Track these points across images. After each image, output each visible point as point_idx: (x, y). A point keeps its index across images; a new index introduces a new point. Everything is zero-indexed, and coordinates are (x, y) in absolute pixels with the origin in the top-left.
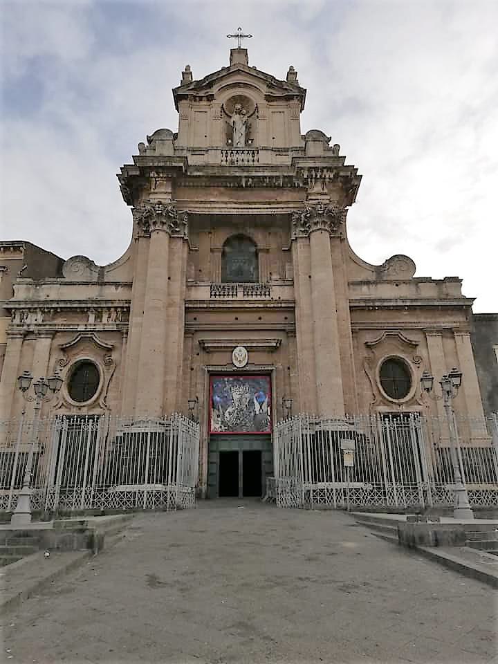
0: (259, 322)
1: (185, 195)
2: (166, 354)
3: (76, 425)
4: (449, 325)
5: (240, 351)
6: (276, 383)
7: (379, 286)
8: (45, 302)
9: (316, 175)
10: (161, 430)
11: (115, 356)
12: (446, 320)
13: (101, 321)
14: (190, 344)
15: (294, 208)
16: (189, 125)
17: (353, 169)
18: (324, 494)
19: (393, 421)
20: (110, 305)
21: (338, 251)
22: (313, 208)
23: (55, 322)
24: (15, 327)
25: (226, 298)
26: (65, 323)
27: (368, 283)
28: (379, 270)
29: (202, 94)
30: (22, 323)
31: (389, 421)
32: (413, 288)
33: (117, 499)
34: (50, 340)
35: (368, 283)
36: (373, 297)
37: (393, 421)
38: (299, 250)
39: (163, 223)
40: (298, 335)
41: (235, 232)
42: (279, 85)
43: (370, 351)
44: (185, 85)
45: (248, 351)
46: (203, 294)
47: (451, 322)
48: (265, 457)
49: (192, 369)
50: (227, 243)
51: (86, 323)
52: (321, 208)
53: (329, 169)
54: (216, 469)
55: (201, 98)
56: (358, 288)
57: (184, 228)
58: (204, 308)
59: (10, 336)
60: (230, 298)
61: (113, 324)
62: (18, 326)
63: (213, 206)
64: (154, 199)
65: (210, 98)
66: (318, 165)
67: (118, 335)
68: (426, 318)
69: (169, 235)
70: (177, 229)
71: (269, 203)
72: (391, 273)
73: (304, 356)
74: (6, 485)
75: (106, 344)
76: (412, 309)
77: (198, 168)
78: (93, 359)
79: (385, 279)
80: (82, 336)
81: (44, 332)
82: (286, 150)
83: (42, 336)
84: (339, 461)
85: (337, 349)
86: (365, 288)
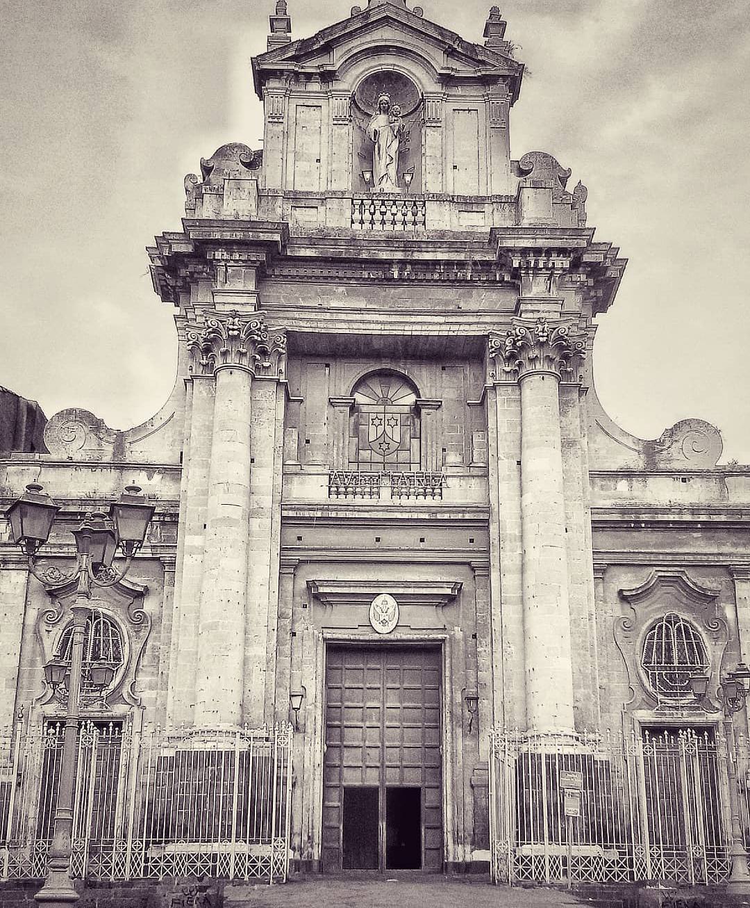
0: (422, 546)
1: (279, 294)
7: (650, 480)
9: (536, 262)
10: (240, 746)
11: (149, 606)
15: (494, 324)
16: (286, 134)
17: (611, 250)
19: (651, 741)
21: (573, 412)
25: (358, 500)
27: (628, 474)
28: (651, 449)
32: (714, 484)
35: (628, 474)
37: (651, 741)
38: (501, 411)
39: (242, 354)
40: (494, 575)
41: (374, 367)
42: (469, 53)
43: (627, 606)
44: (278, 46)
48: (428, 799)
53: (562, 251)
55: (309, 77)
57: (280, 360)
60: (367, 500)
64: (226, 303)
65: (327, 77)
66: (540, 243)
67: (154, 566)
68: (735, 545)
69: (249, 372)
70: (266, 364)
72: (675, 455)
73: (507, 616)
74: (155, 836)
75: (134, 584)
76: (709, 527)
77: (312, 242)
79: (662, 466)
83: (11, 566)
84: (557, 811)
85: (564, 603)
86: (623, 485)
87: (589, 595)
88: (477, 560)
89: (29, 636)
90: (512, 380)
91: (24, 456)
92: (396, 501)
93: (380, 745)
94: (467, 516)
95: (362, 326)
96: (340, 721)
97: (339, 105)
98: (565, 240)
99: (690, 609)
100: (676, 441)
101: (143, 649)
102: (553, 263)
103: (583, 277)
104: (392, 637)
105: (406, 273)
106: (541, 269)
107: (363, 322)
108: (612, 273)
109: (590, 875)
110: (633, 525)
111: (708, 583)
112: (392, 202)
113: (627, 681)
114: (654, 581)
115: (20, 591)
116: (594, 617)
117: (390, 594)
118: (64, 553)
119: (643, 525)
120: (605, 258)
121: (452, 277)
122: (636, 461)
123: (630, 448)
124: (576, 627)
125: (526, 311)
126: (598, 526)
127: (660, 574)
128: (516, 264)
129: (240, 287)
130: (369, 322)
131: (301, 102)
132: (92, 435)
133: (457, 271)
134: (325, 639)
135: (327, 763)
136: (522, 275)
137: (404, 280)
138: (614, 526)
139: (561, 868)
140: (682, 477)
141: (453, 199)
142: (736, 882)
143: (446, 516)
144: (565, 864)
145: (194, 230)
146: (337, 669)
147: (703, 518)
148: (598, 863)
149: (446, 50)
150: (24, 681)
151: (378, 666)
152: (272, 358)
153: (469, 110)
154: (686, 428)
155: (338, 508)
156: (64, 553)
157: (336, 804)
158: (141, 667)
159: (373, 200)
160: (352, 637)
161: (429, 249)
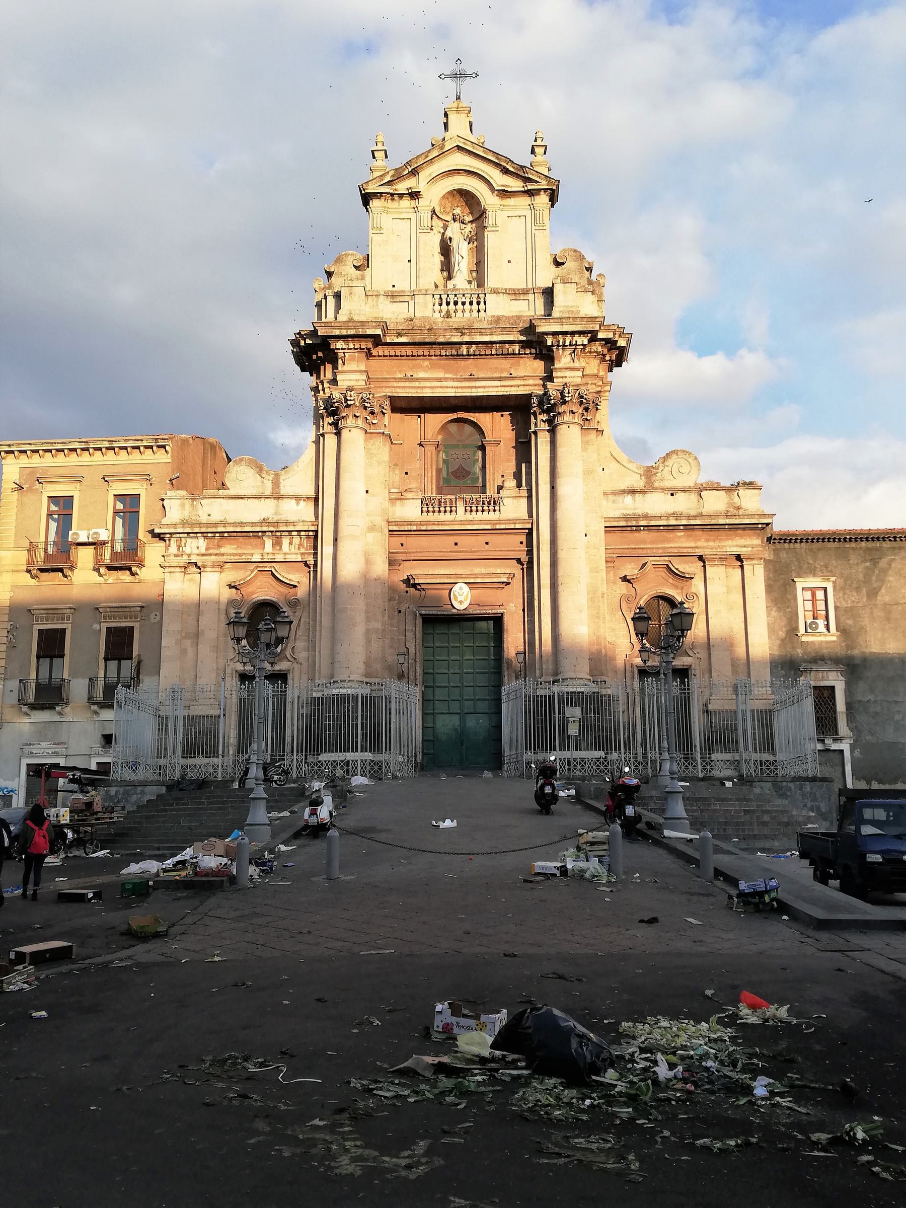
3: (281, 691)
4: (736, 551)
7: (648, 495)
8: (208, 525)
9: (564, 342)
10: (367, 691)
12: (735, 543)
13: (281, 549)
20: (291, 528)
23: (223, 550)
26: (235, 551)
27: (632, 492)
30: (180, 553)
32: (694, 497)
33: (594, 767)
35: (632, 492)
36: (639, 512)
46: (411, 511)
49: (400, 612)
51: (262, 552)
53: (580, 333)
56: (619, 498)
62: (176, 556)
68: (707, 540)
71: (500, 379)
74: (191, 754)
79: (656, 485)
80: (259, 569)
82: (525, 291)
86: (628, 499)
87: (602, 580)
91: (213, 492)
93: (460, 685)
94: (518, 526)
95: (441, 390)
100: (667, 466)
102: (576, 341)
103: (600, 349)
106: (567, 346)
108: (622, 343)
111: (688, 568)
117: (465, 583)
120: (615, 334)
121: (505, 352)
122: (638, 482)
125: (557, 377)
126: (609, 529)
128: (549, 343)
130: (447, 387)
132: (257, 475)
134: (421, 615)
135: (425, 698)
139: (567, 767)
141: (506, 291)
142: (662, 776)
143: (503, 527)
144: (569, 764)
145: (321, 329)
146: (430, 634)
147: (684, 522)
148: (327, 765)
149: (502, 170)
153: (520, 216)
154: (674, 456)
155: (427, 523)
158: (297, 636)
161: (488, 333)
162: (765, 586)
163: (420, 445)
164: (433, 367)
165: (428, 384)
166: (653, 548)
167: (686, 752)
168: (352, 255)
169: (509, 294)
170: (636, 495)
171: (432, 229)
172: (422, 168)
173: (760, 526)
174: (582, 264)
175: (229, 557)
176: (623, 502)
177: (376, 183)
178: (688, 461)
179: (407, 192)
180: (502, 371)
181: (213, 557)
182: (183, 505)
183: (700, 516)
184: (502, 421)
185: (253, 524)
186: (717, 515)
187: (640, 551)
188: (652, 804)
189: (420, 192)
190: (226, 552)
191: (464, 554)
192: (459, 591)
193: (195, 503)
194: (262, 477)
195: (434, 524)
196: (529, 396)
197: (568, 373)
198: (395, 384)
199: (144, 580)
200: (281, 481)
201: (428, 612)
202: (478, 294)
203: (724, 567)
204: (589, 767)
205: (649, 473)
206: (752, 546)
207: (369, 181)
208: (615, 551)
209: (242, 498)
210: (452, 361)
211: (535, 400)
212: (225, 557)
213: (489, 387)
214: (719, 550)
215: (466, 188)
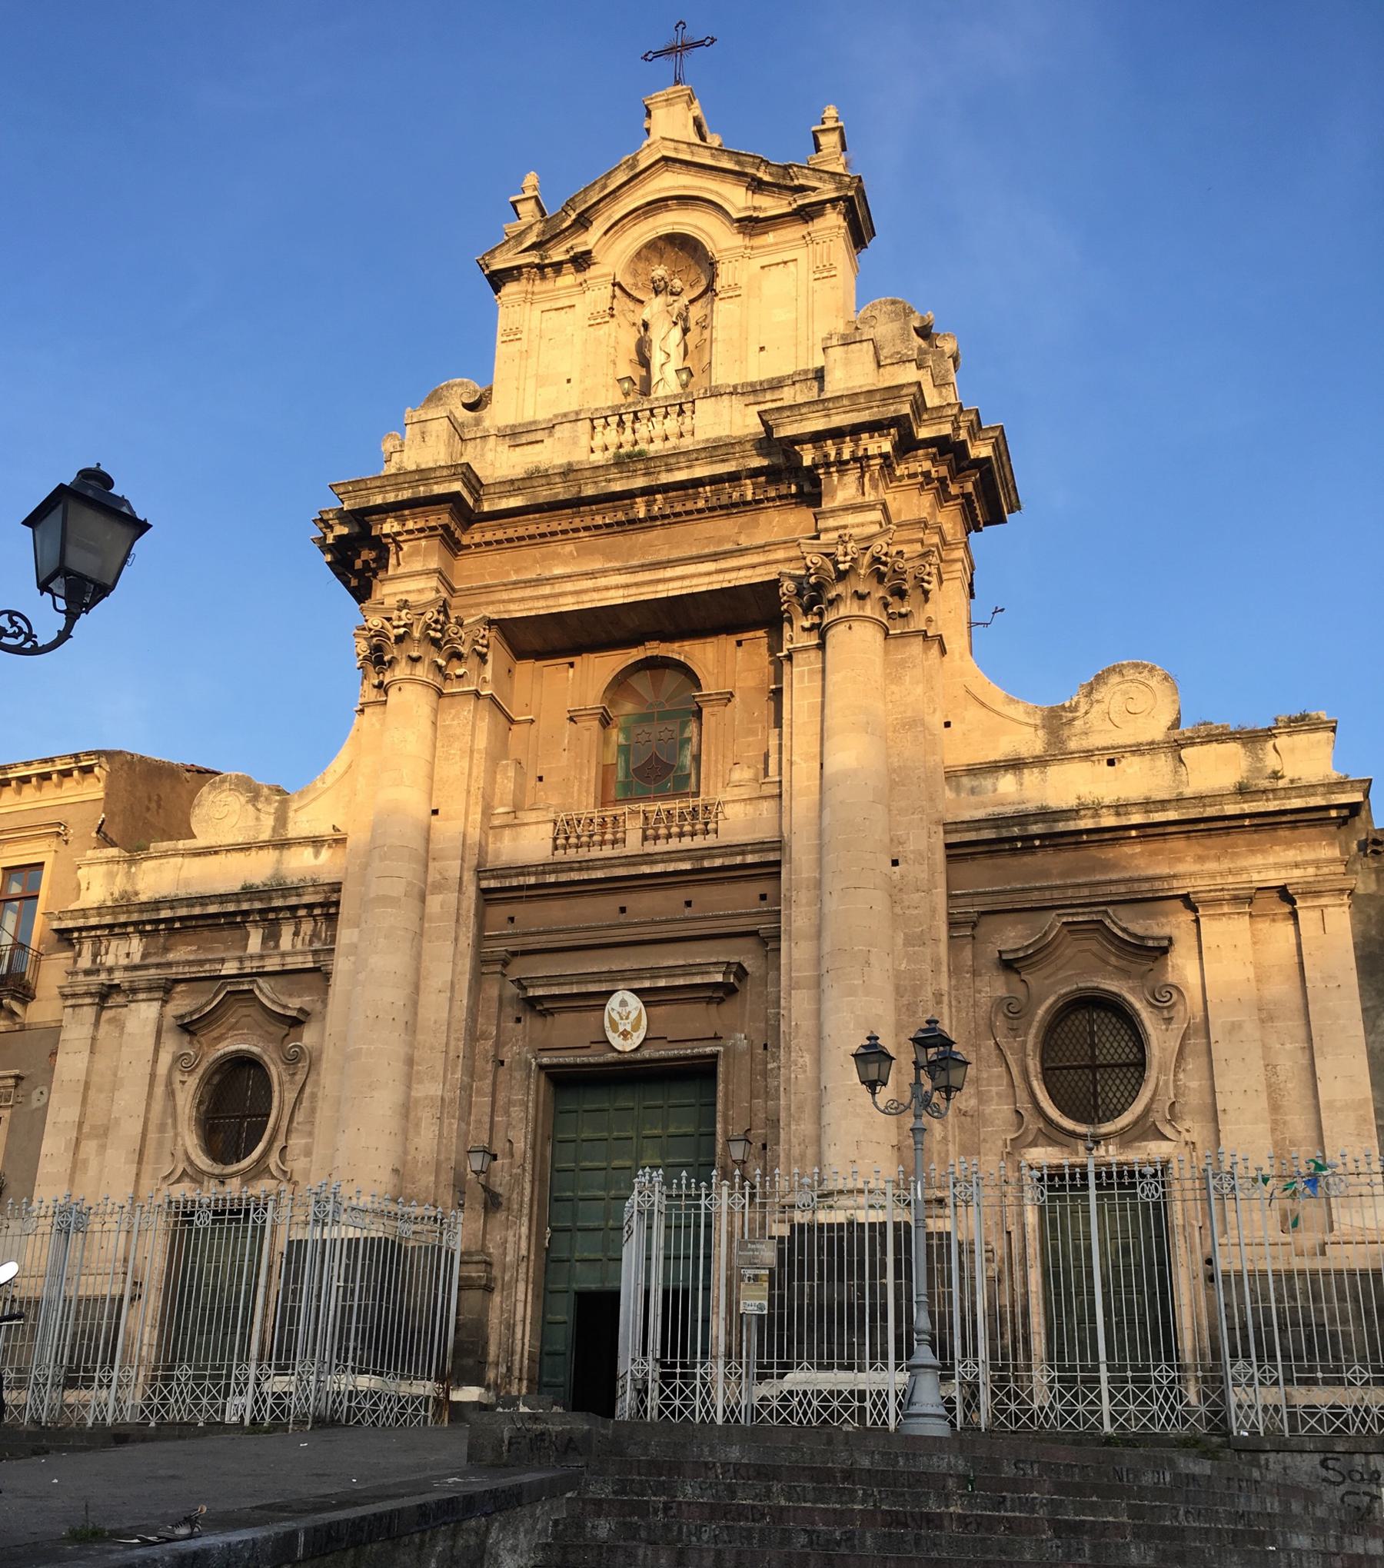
1: (471, 570)
2: (411, 1027)
4: (1275, 878)
5: (623, 1003)
6: (726, 1094)
7: (1053, 771)
9: (839, 453)
12: (1271, 860)
13: (277, 946)
14: (494, 992)
18: (693, 1392)
20: (293, 901)
22: (827, 555)
23: (171, 956)
24: (81, 978)
26: (191, 957)
27: (1015, 765)
29: (557, 254)
30: (95, 967)
31: (732, 1187)
32: (1163, 763)
33: (815, 1403)
34: (156, 1005)
39: (415, 660)
40: (784, 945)
41: (636, 654)
43: (1015, 978)
45: (646, 1004)
47: (1286, 866)
50: (620, 683)
51: (239, 954)
52: (846, 554)
53: (875, 427)
54: (563, 1340)
55: (558, 267)
58: (530, 887)
59: (70, 1002)
60: (608, 851)
61: (303, 953)
63: (558, 589)
65: (582, 261)
66: (839, 420)
68: (1201, 859)
71: (714, 557)
77: (513, 486)
78: (255, 1049)
79: (1073, 745)
80: (229, 988)
81: (143, 985)
82: (775, 383)
83: (142, 996)
87: (936, 962)
88: (764, 926)
89: (160, 1090)
90: (814, 640)
92: (650, 848)
95: (595, 596)
96: (573, 1191)
97: (599, 295)
98: (876, 409)
99: (1124, 973)
100: (1098, 701)
101: (298, 1100)
102: (866, 450)
103: (927, 465)
104: (638, 1056)
105: (656, 508)
107: (596, 590)
108: (981, 450)
109: (1151, 1419)
110: (1019, 845)
112: (648, 412)
113: (1011, 1100)
114: (1054, 932)
115: (151, 1028)
116: (945, 999)
118: (205, 971)
119: (1037, 843)
121: (724, 500)
122: (1030, 742)
123: (1021, 723)
124: (909, 1017)
126: (956, 853)
127: (1065, 920)
128: (807, 461)
129: (418, 566)
130: (607, 588)
131: (547, 306)
132: (250, 807)
133: (730, 490)
136: (822, 477)
137: (655, 518)
138: (991, 848)
140: (1107, 757)
143: (718, 862)
147: (1137, 819)
149: (750, 185)
150: (150, 1151)
151: (631, 1104)
152: (469, 660)
153: (785, 263)
154: (1115, 679)
155: (569, 866)
156: (205, 971)
157: (559, 1318)
159: (620, 415)
160: (578, 1060)
162: (1357, 958)
163: (571, 719)
164: (583, 552)
165: (569, 587)
166: (1066, 887)
167: (1140, 1363)
168: (461, 384)
169: (743, 394)
170: (1025, 771)
171: (612, 316)
172: (597, 211)
173: (1333, 813)
174: (907, 323)
175: (180, 969)
176: (995, 790)
177: (509, 250)
178: (1147, 686)
179: (568, 257)
180: (720, 541)
181: (152, 971)
182: (111, 876)
183: (1180, 801)
184: (739, 654)
185: (222, 898)
186: (1217, 797)
187: (1035, 896)
188: (689, 1490)
189: (589, 252)
190: (177, 958)
191: (639, 929)
192: (620, 1010)
193: (133, 869)
194: (258, 810)
195: (572, 870)
196: (775, 584)
197: (850, 519)
198: (505, 596)
199: (30, 1024)
200: (291, 814)
201: (555, 1061)
202: (681, 405)
203: (1247, 917)
204: (800, 1403)
205: (1056, 722)
206: (1317, 863)
207: (496, 248)
208: (976, 900)
209: (216, 853)
210: (620, 538)
211: (788, 586)
212: (174, 970)
213: (693, 576)
214: (1231, 879)
215: (679, 229)
